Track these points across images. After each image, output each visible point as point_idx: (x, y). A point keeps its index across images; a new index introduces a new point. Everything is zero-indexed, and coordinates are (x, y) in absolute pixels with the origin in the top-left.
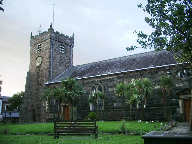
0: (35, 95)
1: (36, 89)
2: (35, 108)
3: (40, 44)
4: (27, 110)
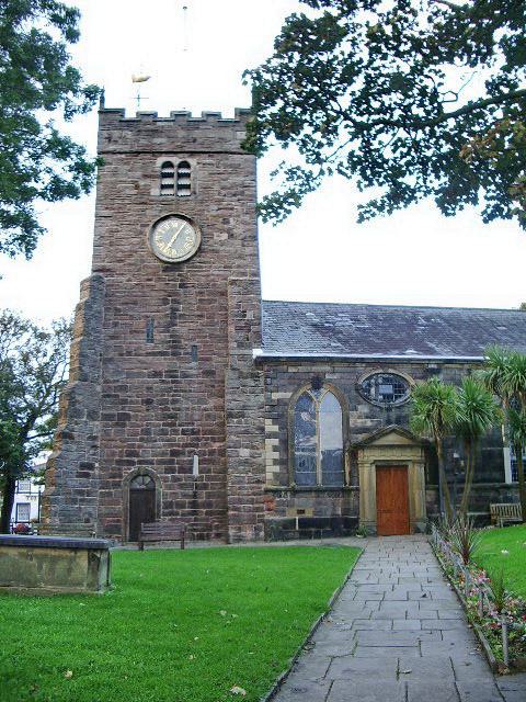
3: (176, 160)
4: (87, 475)
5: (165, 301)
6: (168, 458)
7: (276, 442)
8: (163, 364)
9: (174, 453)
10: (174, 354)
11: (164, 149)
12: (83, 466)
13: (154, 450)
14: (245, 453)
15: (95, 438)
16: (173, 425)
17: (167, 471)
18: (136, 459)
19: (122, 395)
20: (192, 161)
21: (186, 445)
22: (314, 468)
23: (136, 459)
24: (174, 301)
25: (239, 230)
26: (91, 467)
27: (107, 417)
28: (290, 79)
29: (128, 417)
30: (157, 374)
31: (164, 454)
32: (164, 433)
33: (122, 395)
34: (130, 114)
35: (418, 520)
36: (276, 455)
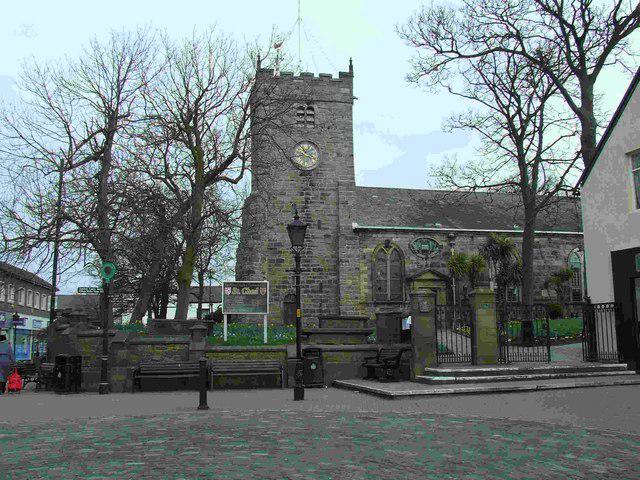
5: (302, 194)
7: (365, 276)
21: (314, 278)
24: (307, 194)
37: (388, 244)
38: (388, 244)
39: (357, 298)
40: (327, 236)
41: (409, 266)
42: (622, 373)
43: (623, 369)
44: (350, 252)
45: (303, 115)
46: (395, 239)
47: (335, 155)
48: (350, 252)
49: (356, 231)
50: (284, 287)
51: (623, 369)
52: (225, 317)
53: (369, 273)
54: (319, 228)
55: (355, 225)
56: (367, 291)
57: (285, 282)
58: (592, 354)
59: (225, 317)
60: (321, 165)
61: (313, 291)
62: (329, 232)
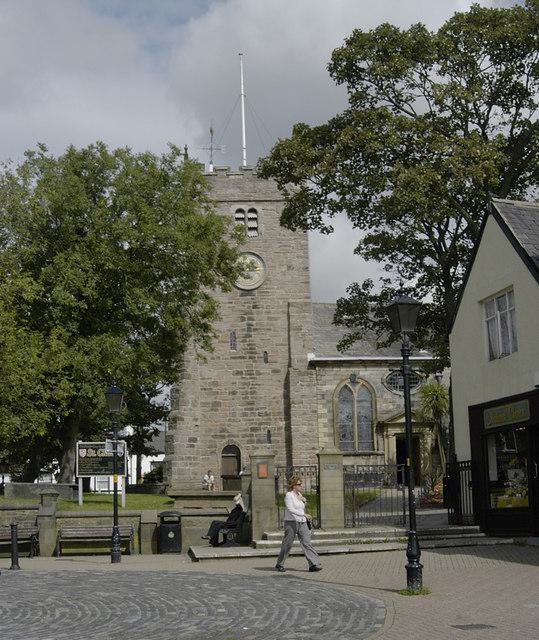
0: (234, 393)
1: (239, 373)
2: (239, 441)
3: (246, 207)
4: (193, 446)
5: (243, 319)
6: (249, 433)
7: (326, 420)
8: (242, 366)
9: (253, 429)
10: (250, 358)
11: (237, 198)
12: (191, 440)
13: (241, 425)
14: (304, 429)
15: (196, 420)
16: (252, 409)
17: (248, 442)
18: (226, 434)
19: (215, 389)
20: (258, 208)
21: (261, 424)
22: (353, 438)
23: (226, 434)
24: (250, 319)
25: (296, 262)
26: (195, 440)
27: (205, 404)
28: (515, 63)
29: (219, 404)
30: (239, 373)
31: (245, 430)
32: (245, 415)
33: (215, 389)
34: (433, 27)
35: (77, 320)
36: (326, 430)
37: (354, 379)
38: (354, 379)
39: (313, 448)
40: (276, 371)
41: (382, 406)
42: (476, 535)
43: (476, 531)
44: (305, 391)
45: (243, 219)
46: (363, 372)
47: (285, 268)
48: (305, 391)
49: (313, 364)
50: (223, 437)
51: (476, 531)
52: (391, 264)
53: (330, 416)
54: (266, 361)
55: (311, 357)
56: (326, 439)
57: (223, 431)
58: (456, 518)
59: (391, 264)
60: (267, 280)
61: (259, 441)
62: (277, 366)
